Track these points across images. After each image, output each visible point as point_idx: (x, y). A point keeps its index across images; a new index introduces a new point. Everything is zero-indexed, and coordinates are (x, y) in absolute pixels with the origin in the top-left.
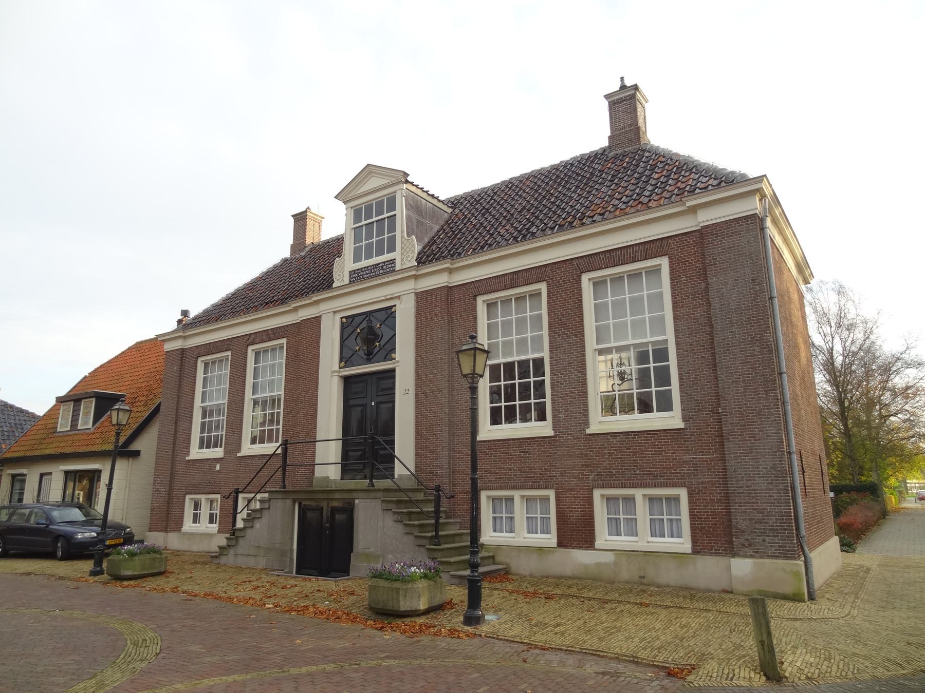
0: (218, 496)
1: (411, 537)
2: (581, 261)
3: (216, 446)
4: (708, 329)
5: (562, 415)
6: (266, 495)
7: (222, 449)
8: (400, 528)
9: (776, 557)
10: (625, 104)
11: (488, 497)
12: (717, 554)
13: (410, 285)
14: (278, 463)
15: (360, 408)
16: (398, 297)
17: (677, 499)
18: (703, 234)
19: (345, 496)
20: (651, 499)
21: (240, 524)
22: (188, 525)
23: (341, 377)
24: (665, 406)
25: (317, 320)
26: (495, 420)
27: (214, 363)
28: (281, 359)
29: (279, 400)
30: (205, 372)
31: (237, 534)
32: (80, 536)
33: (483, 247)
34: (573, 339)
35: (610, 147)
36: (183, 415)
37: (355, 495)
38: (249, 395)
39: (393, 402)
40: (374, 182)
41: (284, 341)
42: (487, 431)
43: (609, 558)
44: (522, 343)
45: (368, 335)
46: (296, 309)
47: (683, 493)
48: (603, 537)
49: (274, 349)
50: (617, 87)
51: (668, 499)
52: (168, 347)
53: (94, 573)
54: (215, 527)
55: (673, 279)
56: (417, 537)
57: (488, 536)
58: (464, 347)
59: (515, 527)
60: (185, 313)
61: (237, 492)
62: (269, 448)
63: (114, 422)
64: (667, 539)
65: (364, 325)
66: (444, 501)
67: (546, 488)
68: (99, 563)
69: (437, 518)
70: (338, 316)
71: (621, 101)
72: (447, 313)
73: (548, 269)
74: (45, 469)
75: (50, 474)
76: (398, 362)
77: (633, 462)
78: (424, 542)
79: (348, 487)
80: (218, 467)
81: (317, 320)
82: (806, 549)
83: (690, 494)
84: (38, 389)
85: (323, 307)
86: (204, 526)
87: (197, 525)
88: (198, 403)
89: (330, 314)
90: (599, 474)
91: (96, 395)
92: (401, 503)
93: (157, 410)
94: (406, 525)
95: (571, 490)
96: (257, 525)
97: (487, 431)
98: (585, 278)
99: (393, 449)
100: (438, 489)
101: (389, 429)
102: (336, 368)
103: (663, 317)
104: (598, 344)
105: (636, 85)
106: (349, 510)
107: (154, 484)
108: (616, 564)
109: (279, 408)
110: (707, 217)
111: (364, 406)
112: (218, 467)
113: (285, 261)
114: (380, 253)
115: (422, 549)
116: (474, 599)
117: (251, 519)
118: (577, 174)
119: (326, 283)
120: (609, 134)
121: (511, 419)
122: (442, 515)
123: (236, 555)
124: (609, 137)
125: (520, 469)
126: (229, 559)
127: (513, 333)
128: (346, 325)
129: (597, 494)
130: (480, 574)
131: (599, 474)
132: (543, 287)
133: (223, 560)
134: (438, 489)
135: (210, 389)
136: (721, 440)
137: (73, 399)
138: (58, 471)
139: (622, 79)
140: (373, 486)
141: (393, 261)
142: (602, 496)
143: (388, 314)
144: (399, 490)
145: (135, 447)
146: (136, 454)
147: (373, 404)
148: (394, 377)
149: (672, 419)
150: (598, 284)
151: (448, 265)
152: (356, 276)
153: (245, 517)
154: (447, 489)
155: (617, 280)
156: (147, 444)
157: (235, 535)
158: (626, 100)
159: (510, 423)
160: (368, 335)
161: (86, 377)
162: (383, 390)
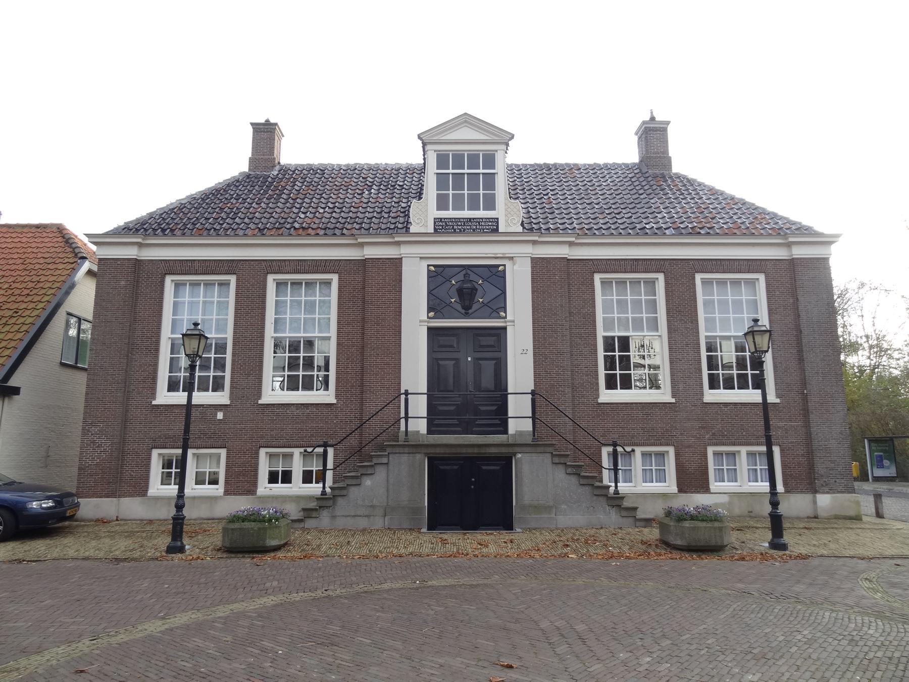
1: (587, 488)
9: (843, 492)
11: (194, 454)
12: (802, 492)
16: (511, 258)
18: (364, 263)
19: (504, 450)
30: (176, 295)
32: (35, 505)
34: (689, 325)
43: (725, 499)
48: (714, 486)
51: (728, 454)
60: (653, 119)
64: (655, 484)
67: (667, 445)
70: (424, 264)
79: (432, 442)
80: (220, 416)
90: (714, 434)
95: (689, 447)
104: (172, 333)
108: (730, 503)
110: (371, 252)
112: (220, 416)
123: (334, 517)
125: (643, 429)
131: (714, 434)
136: (806, 413)
145: (13, 382)
146: (16, 391)
147: (469, 359)
149: (327, 396)
150: (280, 284)
151: (140, 240)
152: (443, 227)
155: (296, 284)
160: (466, 290)
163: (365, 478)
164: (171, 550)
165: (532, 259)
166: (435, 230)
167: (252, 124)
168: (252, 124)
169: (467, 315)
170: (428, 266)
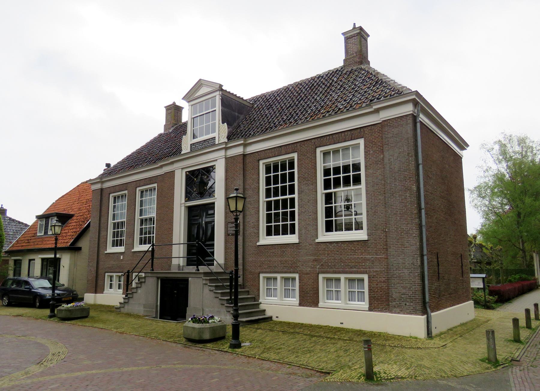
1: (212, 293)
2: (316, 140)
3: (121, 245)
4: (383, 182)
5: (303, 231)
8: (212, 295)
10: (357, 40)
11: (264, 277)
13: (222, 153)
14: (149, 255)
16: (217, 160)
17: (362, 280)
23: (186, 207)
26: (269, 233)
27: (147, 191)
30: (115, 202)
33: (265, 131)
34: (311, 187)
35: (344, 66)
37: (192, 275)
38: (137, 217)
40: (204, 90)
41: (156, 185)
45: (198, 182)
46: (161, 167)
47: (366, 277)
50: (351, 28)
52: (94, 187)
53: (51, 317)
55: (366, 152)
58: (232, 195)
60: (108, 165)
62: (146, 247)
67: (294, 272)
68: (52, 311)
71: (351, 37)
73: (298, 145)
74: (32, 257)
75: (34, 260)
76: (216, 199)
81: (172, 173)
82: (429, 310)
83: (369, 277)
84: (26, 211)
85: (176, 165)
88: (111, 221)
90: (322, 265)
91: (58, 216)
93: (89, 226)
94: (215, 293)
95: (307, 274)
98: (318, 150)
101: (212, 238)
102: (183, 201)
110: (385, 115)
113: (160, 135)
114: (207, 133)
118: (324, 84)
119: (177, 150)
121: (277, 233)
122: (236, 289)
125: (281, 261)
126: (127, 309)
129: (321, 276)
131: (322, 265)
132: (361, 142)
133: (122, 310)
135: (118, 211)
137: (45, 217)
138: (38, 259)
141: (214, 138)
148: (214, 207)
149: (361, 235)
151: (242, 142)
156: (85, 244)
158: (354, 36)
163: (139, 289)
165: (226, 158)
167: (183, 99)
168: (183, 99)
170: (186, 172)
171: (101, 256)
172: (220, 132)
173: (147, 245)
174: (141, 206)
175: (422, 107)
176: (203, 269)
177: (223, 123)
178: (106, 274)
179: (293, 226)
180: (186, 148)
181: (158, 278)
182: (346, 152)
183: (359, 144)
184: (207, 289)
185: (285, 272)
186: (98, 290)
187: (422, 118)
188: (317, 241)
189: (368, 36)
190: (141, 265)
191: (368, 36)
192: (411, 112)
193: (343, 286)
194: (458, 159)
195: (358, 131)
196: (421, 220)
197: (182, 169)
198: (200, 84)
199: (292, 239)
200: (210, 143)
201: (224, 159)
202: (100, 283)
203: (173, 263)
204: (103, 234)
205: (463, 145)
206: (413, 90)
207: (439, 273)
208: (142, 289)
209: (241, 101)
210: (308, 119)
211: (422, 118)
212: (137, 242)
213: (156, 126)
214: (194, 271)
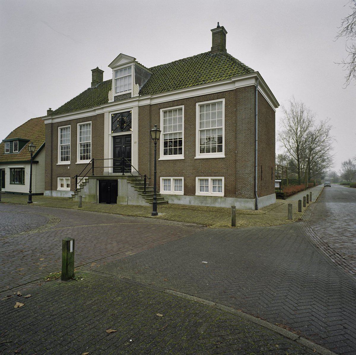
0: (70, 178)
1: (133, 188)
2: (196, 98)
3: (67, 160)
4: (235, 125)
6: (87, 178)
7: (70, 161)
10: (220, 34)
13: (136, 103)
15: (119, 148)
16: (132, 108)
17: (221, 180)
20: (213, 180)
21: (78, 187)
22: (59, 188)
23: (112, 136)
24: (220, 150)
25: (103, 115)
28: (90, 129)
29: (90, 144)
31: (78, 190)
36: (54, 148)
37: (119, 178)
38: (78, 142)
39: (131, 146)
40: (123, 61)
41: (91, 122)
42: (163, 157)
44: (175, 127)
45: (122, 121)
46: (95, 110)
47: (223, 178)
48: (198, 193)
49: (87, 125)
52: (46, 122)
54: (69, 189)
56: (138, 191)
57: (162, 192)
58: (153, 130)
59: (170, 188)
61: (77, 176)
63: (30, 151)
65: (120, 117)
66: (147, 180)
69: (145, 185)
72: (149, 114)
73: (185, 100)
76: (132, 132)
77: (208, 168)
78: (141, 193)
81: (103, 115)
86: (65, 188)
87: (63, 188)
89: (108, 112)
92: (133, 180)
93: (44, 145)
96: (85, 187)
97: (163, 157)
98: (197, 104)
99: (131, 163)
100: (145, 176)
101: (129, 156)
102: (110, 133)
103: (222, 119)
105: (223, 26)
106: (116, 181)
107: (45, 173)
109: (90, 147)
111: (121, 147)
113: (89, 89)
115: (140, 195)
116: (155, 209)
117: (82, 186)
119: (105, 101)
120: (212, 46)
121: (171, 153)
122: (147, 186)
124: (212, 48)
127: (171, 126)
128: (113, 117)
129: (197, 178)
130: (157, 202)
132: (223, 100)
134: (145, 176)
135: (64, 139)
139: (218, 23)
140: (124, 175)
142: (199, 179)
143: (129, 114)
144: (133, 176)
145: (37, 159)
146: (37, 162)
147: (124, 146)
149: (222, 155)
151: (150, 97)
152: (117, 98)
153: (80, 185)
154: (148, 176)
156: (41, 159)
157: (77, 191)
159: (175, 154)
161: (12, 132)
162: (127, 141)
163: (84, 186)
164: (29, 203)
165: (139, 107)
166: (115, 100)
169: (122, 131)
170: (112, 114)
171: (54, 167)
172: (135, 89)
173: (89, 160)
174: (61, 138)
175: (259, 82)
176: (126, 174)
177: (136, 84)
178: (58, 178)
179: (181, 149)
180: (111, 99)
181: (97, 179)
182: (202, 108)
183: (222, 101)
184: (129, 186)
185: (176, 176)
186: (53, 188)
187: (259, 88)
188: (195, 158)
189: (227, 33)
190: (85, 172)
191: (227, 33)
192: (254, 84)
193: (172, 183)
194: (274, 113)
195: (222, 93)
196: (255, 147)
197: (109, 112)
198: (121, 56)
199: (181, 157)
200: (127, 96)
201: (138, 107)
202: (54, 183)
203: (105, 171)
204: (54, 152)
205: (277, 105)
206: (255, 71)
207: (262, 177)
208: (86, 186)
209: (144, 69)
210: (175, 88)
211: (259, 88)
212: (59, 159)
213: (85, 83)
214: (121, 175)
